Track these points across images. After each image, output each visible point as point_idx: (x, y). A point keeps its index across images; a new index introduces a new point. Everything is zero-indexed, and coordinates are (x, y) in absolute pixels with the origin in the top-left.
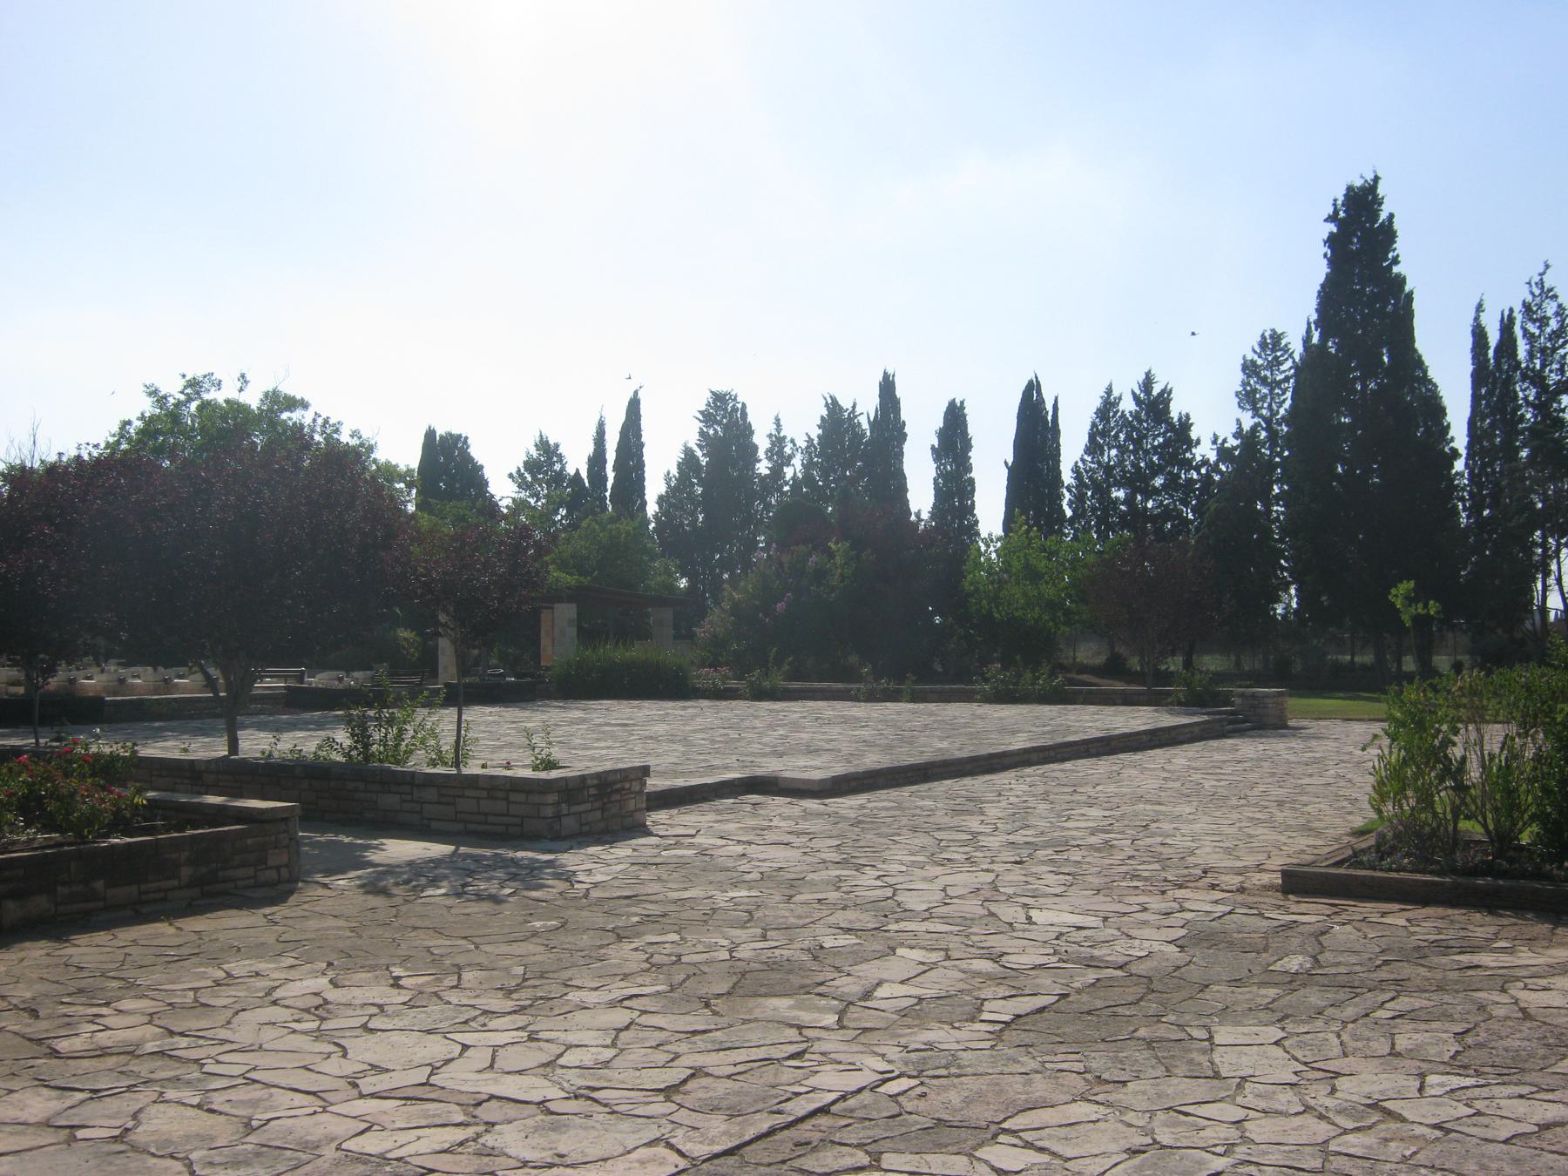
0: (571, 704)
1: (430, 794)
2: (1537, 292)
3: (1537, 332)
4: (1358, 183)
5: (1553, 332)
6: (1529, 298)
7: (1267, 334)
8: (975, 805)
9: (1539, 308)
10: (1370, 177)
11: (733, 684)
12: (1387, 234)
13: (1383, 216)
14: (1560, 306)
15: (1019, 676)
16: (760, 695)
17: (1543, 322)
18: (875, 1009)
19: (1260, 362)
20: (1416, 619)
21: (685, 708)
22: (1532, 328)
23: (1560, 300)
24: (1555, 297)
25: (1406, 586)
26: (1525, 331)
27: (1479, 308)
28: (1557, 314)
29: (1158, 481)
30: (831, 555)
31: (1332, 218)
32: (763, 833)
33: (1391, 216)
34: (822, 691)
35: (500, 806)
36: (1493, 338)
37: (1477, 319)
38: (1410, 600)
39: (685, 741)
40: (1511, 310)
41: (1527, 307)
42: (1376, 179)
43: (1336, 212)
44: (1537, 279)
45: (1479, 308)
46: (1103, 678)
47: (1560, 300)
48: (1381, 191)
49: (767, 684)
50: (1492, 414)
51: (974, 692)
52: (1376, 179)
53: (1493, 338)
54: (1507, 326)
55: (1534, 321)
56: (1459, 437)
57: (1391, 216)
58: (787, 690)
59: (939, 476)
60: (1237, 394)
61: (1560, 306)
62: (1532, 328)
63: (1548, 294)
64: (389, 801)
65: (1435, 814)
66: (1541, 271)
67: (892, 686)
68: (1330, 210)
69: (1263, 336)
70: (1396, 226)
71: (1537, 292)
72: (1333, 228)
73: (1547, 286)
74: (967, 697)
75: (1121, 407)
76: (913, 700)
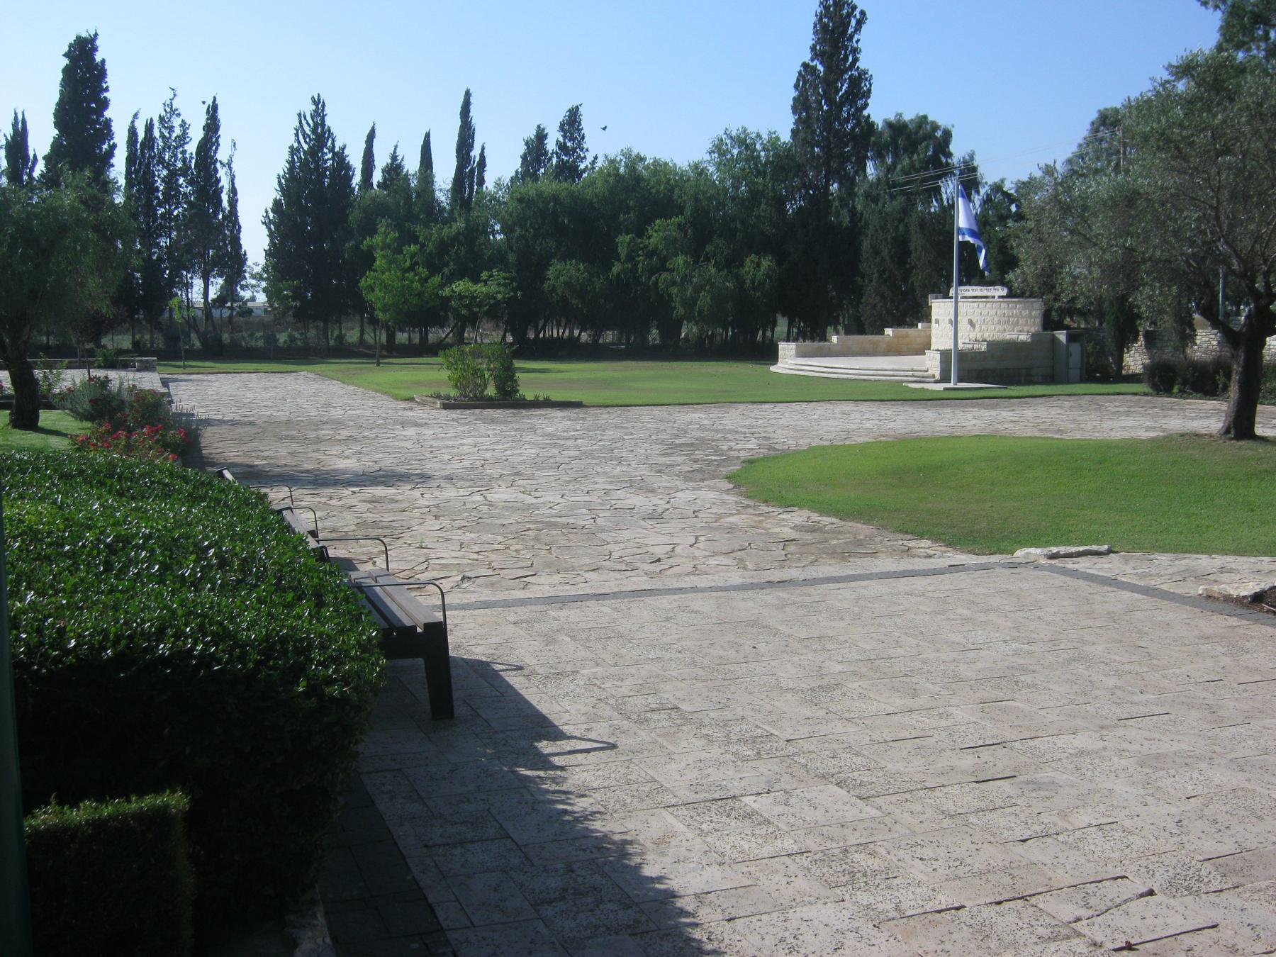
2: (168, 110)
3: (167, 135)
4: (84, 35)
5: (177, 136)
6: (163, 113)
7: (1132, 98)
8: (627, 414)
9: (169, 120)
10: (92, 33)
14: (183, 121)
17: (171, 129)
18: (1108, 394)
21: (25, 434)
24: (179, 115)
27: (136, 116)
28: (181, 126)
32: (424, 517)
36: (141, 135)
37: (133, 122)
40: (151, 120)
41: (161, 119)
42: (96, 35)
45: (136, 116)
48: (98, 43)
50: (139, 184)
52: (96, 35)
53: (141, 135)
54: (149, 128)
55: (166, 128)
60: (925, 117)
61: (183, 121)
63: (174, 112)
65: (1268, 190)
66: (172, 97)
71: (168, 110)
73: (174, 107)
75: (186, 147)
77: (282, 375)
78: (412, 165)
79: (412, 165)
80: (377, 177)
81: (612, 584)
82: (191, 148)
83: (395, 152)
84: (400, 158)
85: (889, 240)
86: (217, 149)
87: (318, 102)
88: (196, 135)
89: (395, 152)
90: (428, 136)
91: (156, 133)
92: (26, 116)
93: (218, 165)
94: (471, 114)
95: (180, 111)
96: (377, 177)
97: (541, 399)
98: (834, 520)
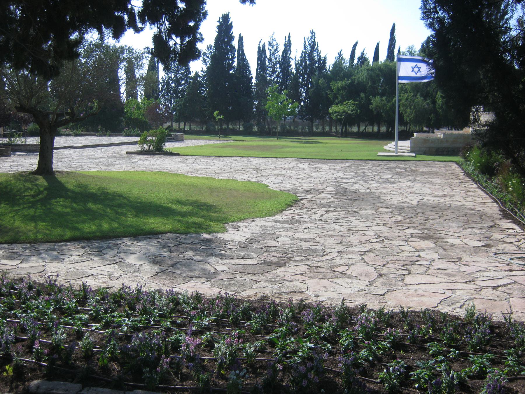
0: (33, 137)
1: (23, 147)
3: (271, 49)
6: (270, 40)
11: (71, 133)
12: (231, 26)
13: (230, 22)
15: (131, 131)
16: (76, 135)
17: (273, 46)
19: (207, 52)
20: (219, 119)
22: (270, 48)
23: (277, 41)
24: (275, 40)
25: (217, 112)
26: (269, 49)
29: (183, 82)
30: (94, 103)
31: (219, 21)
33: (232, 22)
34: (89, 134)
35: (33, 148)
38: (218, 115)
39: (59, 142)
43: (219, 20)
44: (272, 36)
45: (305, 38)
46: (458, 130)
47: (277, 41)
48: (230, 16)
49: (78, 133)
51: (122, 134)
56: (254, 74)
57: (232, 22)
58: (82, 134)
59: (201, 21)
62: (270, 48)
63: (274, 40)
64: (16, 148)
67: (105, 133)
68: (218, 20)
69: (208, 46)
70: (233, 24)
72: (219, 24)
74: (121, 135)
76: (109, 136)
77: (207, 159)
78: (370, 57)
79: (370, 57)
80: (356, 61)
81: (296, 283)
82: (280, 53)
83: (363, 52)
84: (365, 54)
85: (180, 338)
86: (290, 53)
87: (313, 33)
88: (282, 48)
89: (363, 52)
90: (378, 44)
91: (266, 48)
92: (291, 39)
93: (291, 60)
94: (395, 34)
95: (276, 39)
96: (356, 61)
97: (446, 133)
98: (517, 227)
